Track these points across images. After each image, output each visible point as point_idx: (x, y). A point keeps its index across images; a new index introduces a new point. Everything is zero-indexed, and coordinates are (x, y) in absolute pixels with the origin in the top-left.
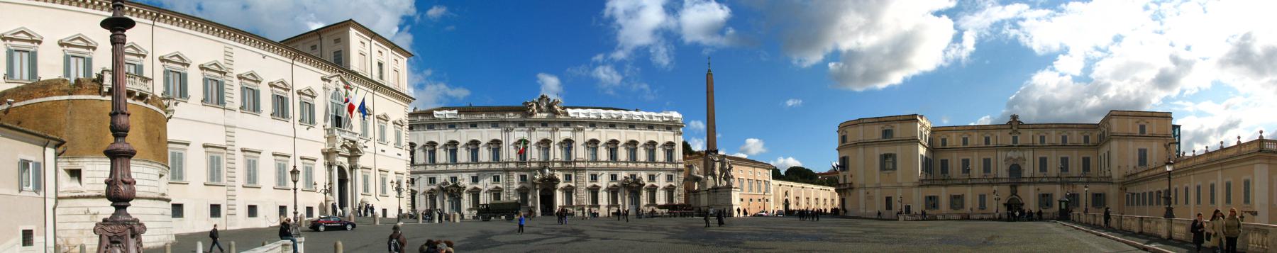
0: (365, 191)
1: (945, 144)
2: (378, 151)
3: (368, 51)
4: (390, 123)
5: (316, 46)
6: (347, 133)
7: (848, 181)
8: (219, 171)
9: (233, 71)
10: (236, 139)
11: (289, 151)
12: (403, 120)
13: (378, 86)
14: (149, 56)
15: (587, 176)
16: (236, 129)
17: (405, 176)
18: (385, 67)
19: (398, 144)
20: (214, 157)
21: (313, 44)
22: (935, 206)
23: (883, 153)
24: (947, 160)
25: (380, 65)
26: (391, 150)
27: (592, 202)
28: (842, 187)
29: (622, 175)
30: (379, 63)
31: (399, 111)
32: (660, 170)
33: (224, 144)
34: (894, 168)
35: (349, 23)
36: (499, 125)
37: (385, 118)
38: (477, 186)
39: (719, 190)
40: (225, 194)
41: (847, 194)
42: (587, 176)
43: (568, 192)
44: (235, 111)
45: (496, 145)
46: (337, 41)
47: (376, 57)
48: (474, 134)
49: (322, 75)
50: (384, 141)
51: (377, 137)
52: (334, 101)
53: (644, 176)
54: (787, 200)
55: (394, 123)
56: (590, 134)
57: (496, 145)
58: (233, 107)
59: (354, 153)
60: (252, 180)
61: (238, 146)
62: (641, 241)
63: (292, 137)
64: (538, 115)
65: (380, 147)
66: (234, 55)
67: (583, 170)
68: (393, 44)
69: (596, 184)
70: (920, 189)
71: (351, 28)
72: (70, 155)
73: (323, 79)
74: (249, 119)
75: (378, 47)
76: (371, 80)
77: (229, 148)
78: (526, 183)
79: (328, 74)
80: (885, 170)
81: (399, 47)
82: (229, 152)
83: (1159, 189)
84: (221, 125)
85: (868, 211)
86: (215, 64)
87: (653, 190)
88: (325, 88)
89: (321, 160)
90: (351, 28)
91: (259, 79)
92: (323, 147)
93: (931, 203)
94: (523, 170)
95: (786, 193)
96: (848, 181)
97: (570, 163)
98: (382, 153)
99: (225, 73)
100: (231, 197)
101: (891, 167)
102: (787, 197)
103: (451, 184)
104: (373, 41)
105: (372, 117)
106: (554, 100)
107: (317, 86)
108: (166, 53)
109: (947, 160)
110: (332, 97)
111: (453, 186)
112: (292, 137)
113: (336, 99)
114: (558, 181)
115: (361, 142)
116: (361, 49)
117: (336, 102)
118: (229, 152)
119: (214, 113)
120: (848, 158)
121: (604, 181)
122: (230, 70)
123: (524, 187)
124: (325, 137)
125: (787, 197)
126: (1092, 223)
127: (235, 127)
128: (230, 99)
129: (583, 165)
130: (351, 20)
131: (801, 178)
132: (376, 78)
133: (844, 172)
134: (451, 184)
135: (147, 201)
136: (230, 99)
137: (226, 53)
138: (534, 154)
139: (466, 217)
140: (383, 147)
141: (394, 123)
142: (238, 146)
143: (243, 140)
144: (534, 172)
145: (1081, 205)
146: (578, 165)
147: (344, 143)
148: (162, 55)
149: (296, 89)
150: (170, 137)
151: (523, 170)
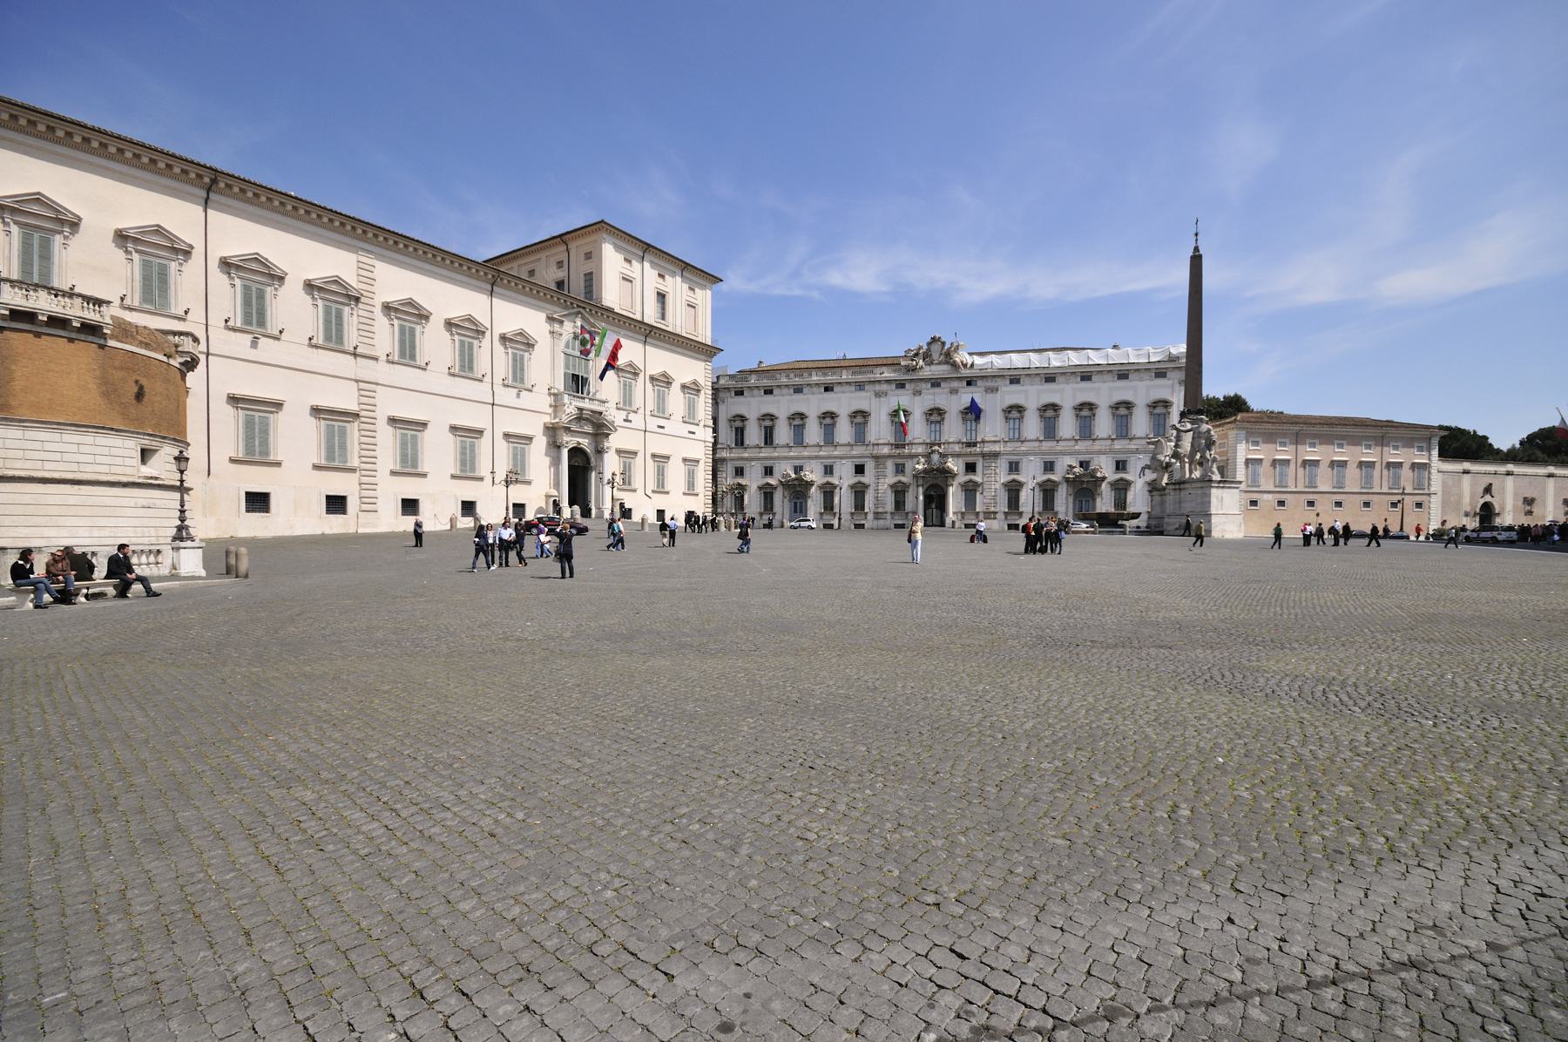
4: (676, 387)
6: (587, 400)
8: (343, 447)
12: (701, 381)
14: (488, 334)
15: (1002, 464)
16: (378, 388)
18: (669, 300)
25: (661, 297)
27: (1009, 507)
29: (1063, 463)
30: (658, 293)
33: (352, 406)
35: (600, 227)
36: (866, 387)
40: (357, 481)
42: (1002, 464)
43: (970, 490)
48: (830, 402)
50: (664, 413)
51: (650, 406)
55: (684, 387)
56: (1011, 394)
57: (860, 418)
58: (373, 353)
59: (600, 428)
60: (409, 466)
61: (382, 414)
62: (636, 955)
63: (213, 355)
64: (927, 368)
65: (653, 423)
67: (996, 455)
69: (1016, 477)
72: (157, 426)
77: (363, 413)
82: (363, 419)
83: (81, 540)
86: (336, 282)
87: (828, 492)
89: (540, 442)
91: (425, 313)
92: (547, 419)
97: (974, 444)
98: (691, 436)
99: (357, 300)
100: (367, 486)
102: (1488, 498)
103: (793, 476)
105: (486, 341)
108: (392, 297)
111: (796, 479)
112: (213, 355)
114: (952, 475)
116: (659, 286)
118: (363, 419)
121: (1031, 475)
124: (551, 406)
125: (1488, 498)
126: (1394, 529)
127: (377, 384)
129: (996, 448)
130: (602, 221)
131: (1549, 456)
132: (651, 317)
134: (793, 476)
135: (68, 487)
137: (361, 265)
138: (918, 430)
140: (662, 422)
142: (382, 414)
144: (915, 460)
146: (988, 448)
148: (120, 227)
149: (498, 331)
150: (1299, 447)
151: (899, 456)
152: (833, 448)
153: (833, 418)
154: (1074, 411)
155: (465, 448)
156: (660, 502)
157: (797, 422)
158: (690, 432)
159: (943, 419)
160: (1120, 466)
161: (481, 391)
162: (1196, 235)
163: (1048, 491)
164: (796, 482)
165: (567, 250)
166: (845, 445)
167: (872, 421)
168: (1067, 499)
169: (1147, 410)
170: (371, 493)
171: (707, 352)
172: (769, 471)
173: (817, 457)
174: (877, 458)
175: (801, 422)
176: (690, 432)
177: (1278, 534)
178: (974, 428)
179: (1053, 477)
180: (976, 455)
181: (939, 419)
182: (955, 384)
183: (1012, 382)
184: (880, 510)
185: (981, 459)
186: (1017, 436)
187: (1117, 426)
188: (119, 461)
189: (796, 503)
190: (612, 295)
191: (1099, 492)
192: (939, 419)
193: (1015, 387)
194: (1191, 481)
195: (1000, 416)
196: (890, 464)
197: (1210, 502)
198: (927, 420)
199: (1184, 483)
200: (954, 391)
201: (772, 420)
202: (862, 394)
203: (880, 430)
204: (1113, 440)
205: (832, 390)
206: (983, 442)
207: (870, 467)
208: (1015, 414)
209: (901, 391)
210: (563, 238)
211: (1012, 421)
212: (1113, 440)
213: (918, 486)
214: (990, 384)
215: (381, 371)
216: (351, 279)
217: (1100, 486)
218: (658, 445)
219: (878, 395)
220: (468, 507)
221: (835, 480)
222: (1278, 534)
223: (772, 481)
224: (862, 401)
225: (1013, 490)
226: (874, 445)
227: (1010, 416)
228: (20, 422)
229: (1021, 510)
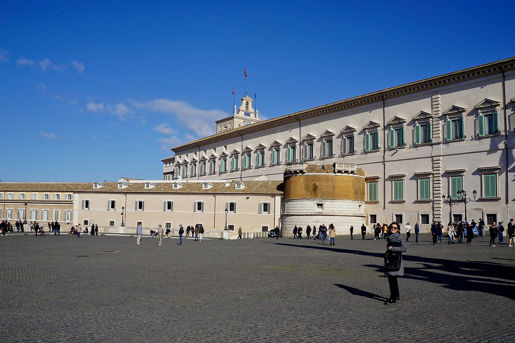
33: (430, 170)
74: (456, 147)
119: (426, 150)
143: (445, 166)
161: (378, 156)
170: (437, 109)
188: (309, 208)
215: (442, 149)
216: (428, 111)
218: (393, 170)
220: (425, 218)
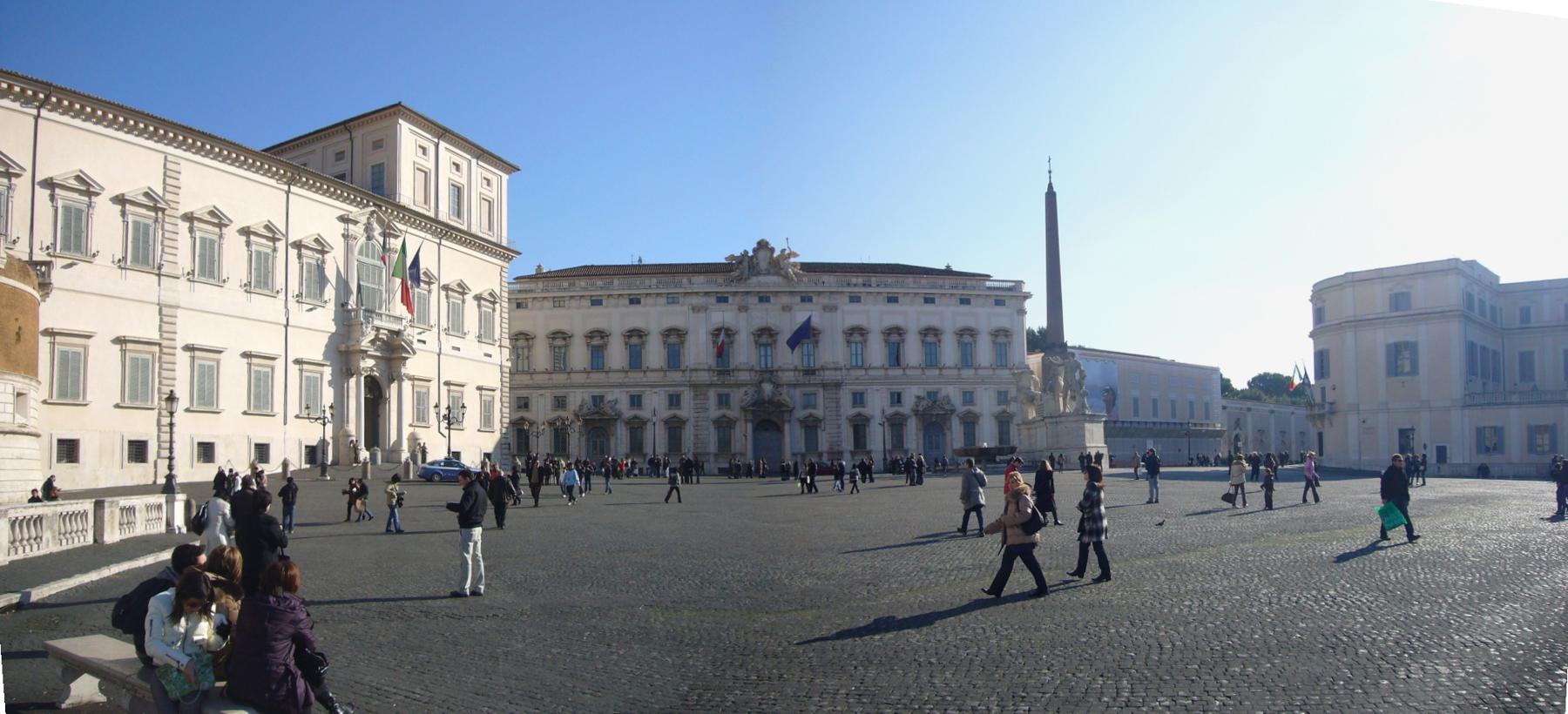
0: (418, 420)
1: (1528, 321)
2: (446, 348)
3: (431, 165)
5: (343, 152)
7: (1328, 399)
8: (145, 383)
9: (179, 207)
10: (178, 328)
11: (276, 348)
13: (444, 231)
16: (179, 310)
17: (497, 394)
19: (484, 336)
20: (204, 366)
21: (339, 148)
22: (1497, 448)
23: (1392, 340)
24: (1531, 353)
26: (470, 346)
28: (1316, 411)
29: (911, 394)
31: (485, 275)
32: (983, 382)
33: (155, 336)
34: (1414, 371)
35: (396, 110)
37: (462, 289)
38: (678, 412)
39: (1063, 419)
41: (1327, 422)
44: (178, 278)
45: (674, 338)
46: (378, 145)
47: (446, 173)
49: (343, 213)
52: (364, 259)
53: (953, 393)
54: (1237, 438)
55: (478, 298)
60: (206, 399)
65: (449, 342)
66: (181, 177)
67: (838, 385)
68: (482, 150)
70: (1466, 412)
71: (401, 121)
73: (344, 219)
74: (205, 293)
75: (450, 154)
76: (436, 221)
78: (729, 408)
79: (353, 211)
80: (1396, 375)
81: (491, 154)
84: (153, 303)
85: (1364, 458)
88: (346, 236)
90: (401, 121)
93: (522, 403)
94: (723, 385)
95: (1238, 423)
96: (1328, 399)
98: (456, 352)
101: (1407, 368)
104: (443, 145)
106: (783, 250)
107: (333, 234)
109: (1531, 353)
110: (361, 253)
113: (367, 256)
115: (411, 334)
117: (369, 261)
118: (165, 350)
119: (142, 283)
120: (1328, 351)
122: (173, 205)
123: (724, 416)
125: (1238, 431)
127: (177, 307)
128: (171, 258)
129: (837, 376)
130: (399, 104)
132: (445, 215)
133: (1322, 380)
136: (171, 258)
138: (744, 353)
139: (36, 416)
140: (456, 342)
141: (478, 298)
145: (525, 396)
146: (829, 376)
147: (376, 335)
152: (642, 374)
153: (640, 336)
154: (661, 337)
155: (260, 379)
156: (262, 430)
157: (596, 341)
158: (454, 348)
159: (775, 342)
160: (636, 401)
162: (1050, 172)
163: (896, 423)
164: (596, 417)
165: (351, 139)
166: (656, 370)
167: (691, 338)
168: (917, 435)
169: (882, 337)
171: (505, 253)
172: (897, 398)
173: (621, 385)
174: (695, 386)
175: (601, 342)
176: (454, 348)
177: (1395, 491)
178: (769, 353)
179: (901, 410)
180: (815, 385)
181: (770, 341)
182: (785, 300)
183: (803, 300)
184: (699, 451)
185: (821, 390)
186: (860, 364)
187: (962, 355)
189: (595, 443)
190: (408, 191)
191: (948, 425)
192: (770, 341)
193: (855, 306)
194: (1064, 415)
195: (840, 339)
196: (712, 393)
197: (1084, 436)
198: (756, 343)
199: (1060, 416)
200: (786, 308)
201: (564, 339)
202: (676, 308)
203: (698, 351)
204: (627, 372)
205: (859, 301)
206: (823, 369)
207: (687, 396)
208: (857, 337)
209: (723, 306)
210: (346, 126)
211: (853, 345)
212: (886, 369)
213: (746, 421)
214: (825, 300)
217: (950, 419)
219: (695, 309)
221: (645, 413)
222: (1395, 491)
223: (568, 414)
224: (676, 316)
225: (860, 426)
226: (692, 370)
227: (852, 339)
228: (1493, 478)
229: (868, 448)
